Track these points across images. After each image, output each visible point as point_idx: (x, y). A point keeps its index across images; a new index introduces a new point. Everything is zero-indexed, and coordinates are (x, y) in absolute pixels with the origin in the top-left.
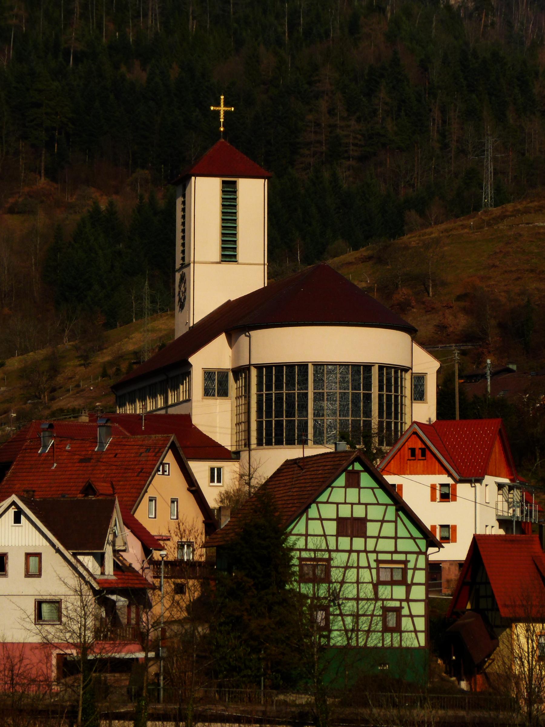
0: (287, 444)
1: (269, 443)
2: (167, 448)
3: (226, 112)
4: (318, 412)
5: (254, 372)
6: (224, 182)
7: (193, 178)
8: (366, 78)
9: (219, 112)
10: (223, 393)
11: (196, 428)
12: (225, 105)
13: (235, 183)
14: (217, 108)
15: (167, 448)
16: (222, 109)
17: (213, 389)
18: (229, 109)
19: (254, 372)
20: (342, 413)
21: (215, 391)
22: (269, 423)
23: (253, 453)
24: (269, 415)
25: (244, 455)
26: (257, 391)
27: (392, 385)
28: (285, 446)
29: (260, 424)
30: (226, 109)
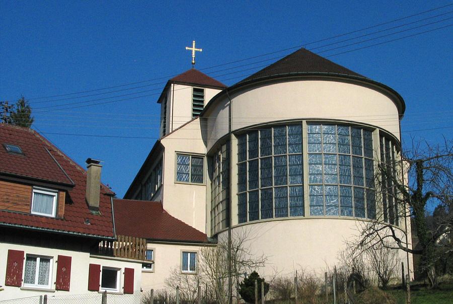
0: (277, 216)
1: (254, 217)
2: (142, 261)
3: (196, 52)
4: (315, 177)
5: (235, 142)
6: (195, 90)
7: (172, 85)
8: (247, 277)
9: (191, 51)
10: (197, 178)
11: (166, 213)
12: (196, 47)
13: (202, 91)
14: (190, 49)
15: (142, 261)
16: (194, 49)
17: (187, 174)
18: (199, 50)
19: (235, 142)
20: (343, 179)
21: (189, 176)
22: (254, 194)
23: (233, 231)
24: (254, 182)
25: (223, 238)
26: (239, 191)
27: (390, 149)
28: (274, 218)
29: (242, 197)
30: (197, 50)
